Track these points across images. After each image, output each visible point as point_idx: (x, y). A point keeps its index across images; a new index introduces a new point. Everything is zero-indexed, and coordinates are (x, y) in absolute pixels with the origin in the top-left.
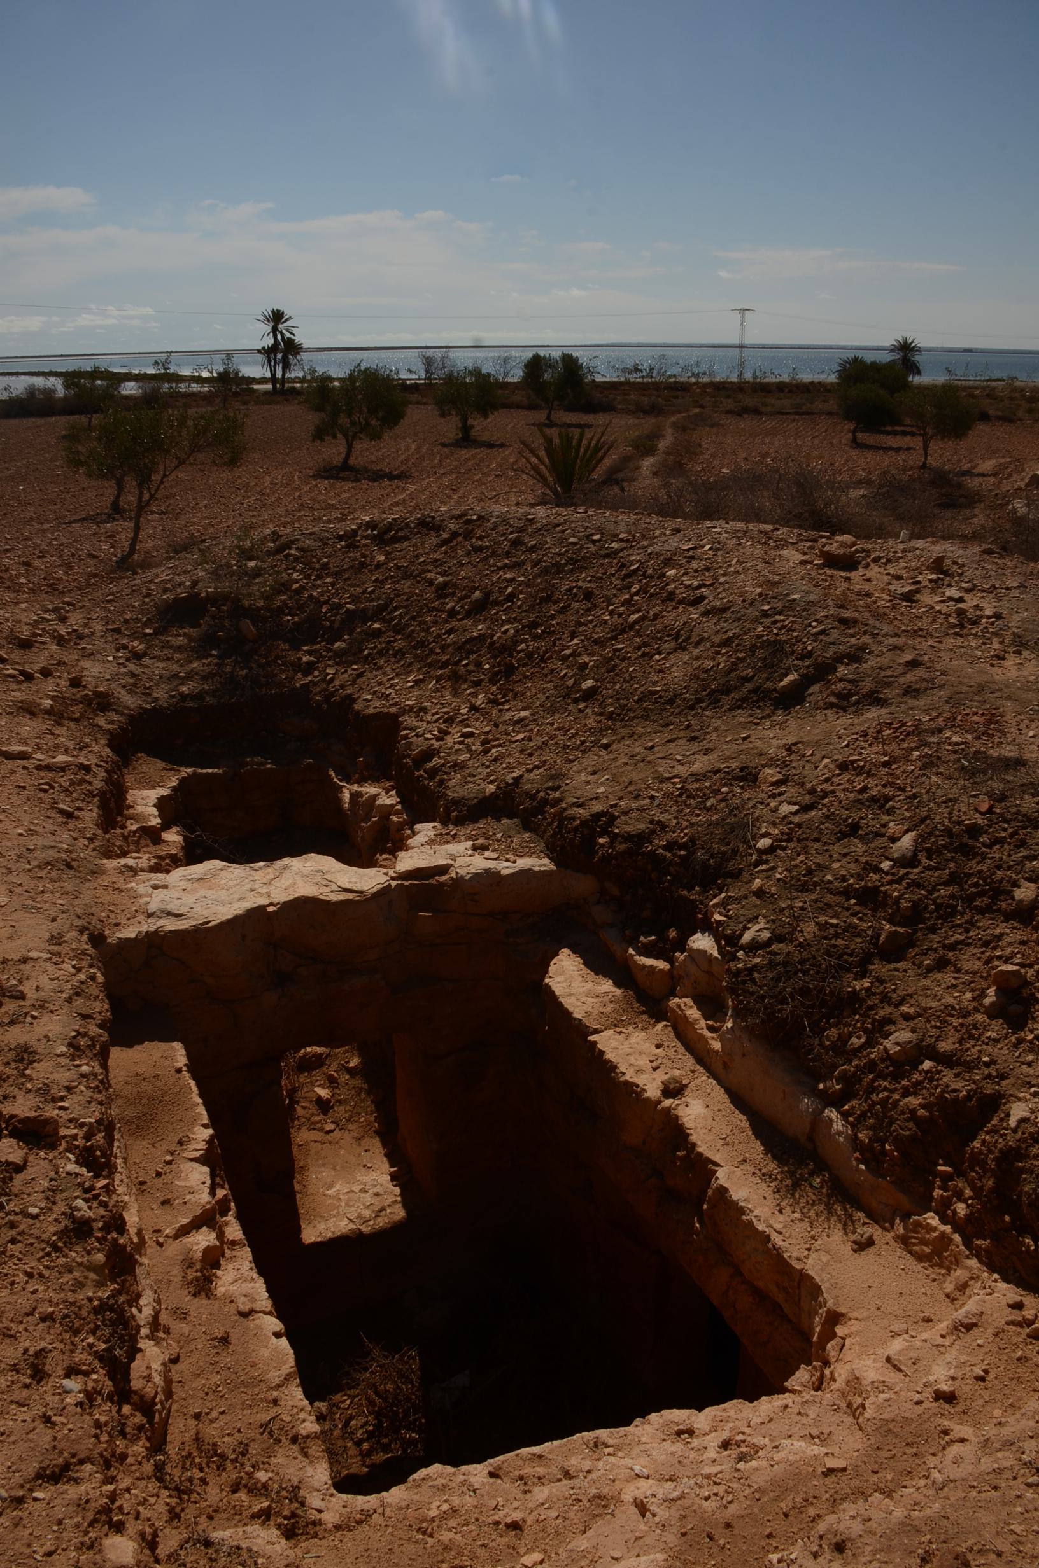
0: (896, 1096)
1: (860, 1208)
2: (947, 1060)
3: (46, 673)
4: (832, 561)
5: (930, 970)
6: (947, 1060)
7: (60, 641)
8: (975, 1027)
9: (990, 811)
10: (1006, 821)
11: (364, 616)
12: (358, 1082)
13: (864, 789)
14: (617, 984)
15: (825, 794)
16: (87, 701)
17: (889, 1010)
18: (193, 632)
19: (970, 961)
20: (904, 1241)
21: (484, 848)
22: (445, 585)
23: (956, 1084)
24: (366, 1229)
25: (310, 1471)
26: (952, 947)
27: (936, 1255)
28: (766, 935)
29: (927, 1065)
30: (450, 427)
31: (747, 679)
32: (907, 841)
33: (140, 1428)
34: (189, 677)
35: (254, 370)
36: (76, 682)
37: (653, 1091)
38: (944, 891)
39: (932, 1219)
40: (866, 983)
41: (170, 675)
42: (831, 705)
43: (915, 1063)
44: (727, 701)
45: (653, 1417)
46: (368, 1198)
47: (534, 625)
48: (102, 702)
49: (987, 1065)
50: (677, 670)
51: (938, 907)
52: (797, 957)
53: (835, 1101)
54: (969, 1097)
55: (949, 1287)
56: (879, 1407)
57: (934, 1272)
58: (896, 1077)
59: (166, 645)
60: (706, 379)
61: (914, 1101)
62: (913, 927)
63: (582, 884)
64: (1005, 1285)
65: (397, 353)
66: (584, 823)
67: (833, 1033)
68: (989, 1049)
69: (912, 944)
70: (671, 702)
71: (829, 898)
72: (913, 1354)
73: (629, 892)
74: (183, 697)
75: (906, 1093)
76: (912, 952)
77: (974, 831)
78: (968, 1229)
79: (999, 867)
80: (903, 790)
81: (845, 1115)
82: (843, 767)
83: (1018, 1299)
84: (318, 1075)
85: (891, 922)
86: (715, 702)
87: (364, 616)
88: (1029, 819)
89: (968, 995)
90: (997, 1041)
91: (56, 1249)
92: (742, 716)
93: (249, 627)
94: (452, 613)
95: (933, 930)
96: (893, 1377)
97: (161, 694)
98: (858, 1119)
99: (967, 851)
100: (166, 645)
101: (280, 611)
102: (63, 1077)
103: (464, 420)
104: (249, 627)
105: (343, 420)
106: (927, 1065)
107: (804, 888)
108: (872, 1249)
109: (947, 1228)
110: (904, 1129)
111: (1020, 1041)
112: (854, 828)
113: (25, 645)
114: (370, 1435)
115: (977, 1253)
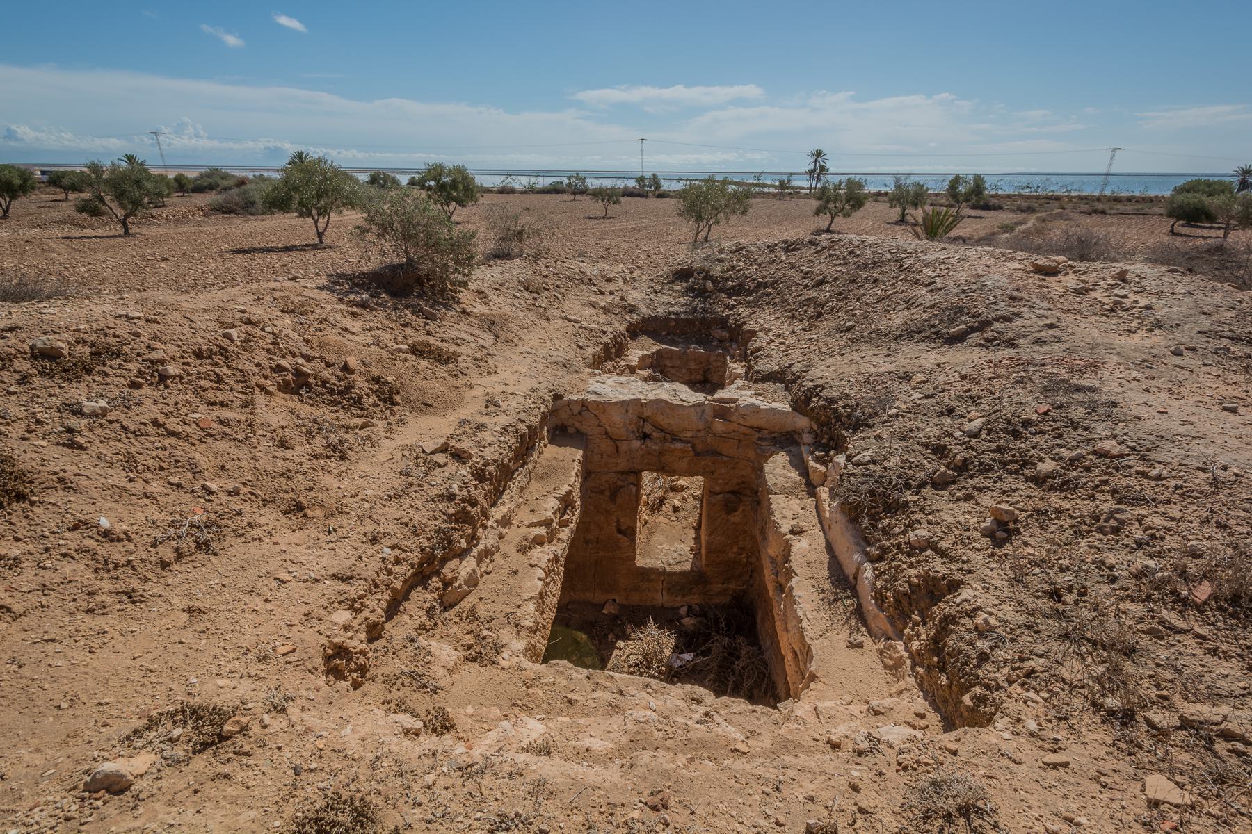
0: (905, 566)
1: (866, 625)
2: (942, 553)
3: (611, 293)
4: (1039, 270)
5: (958, 499)
6: (942, 553)
7: (625, 281)
8: (968, 538)
9: (1046, 413)
10: (1055, 421)
11: (766, 285)
12: (696, 503)
13: (969, 390)
14: (800, 475)
15: (943, 391)
16: (624, 308)
17: (922, 515)
18: (684, 284)
19: (987, 500)
20: (881, 653)
21: (759, 395)
22: (807, 273)
23: (939, 567)
24: (668, 569)
25: (514, 641)
26: (980, 490)
27: (894, 668)
28: (868, 458)
29: (929, 552)
30: (895, 213)
31: (933, 326)
32: (977, 423)
33: (437, 589)
34: (676, 304)
35: (802, 183)
36: (622, 299)
37: (785, 528)
38: (987, 456)
39: (900, 646)
40: (916, 498)
41: (673, 302)
42: (980, 345)
43: (922, 550)
44: (917, 337)
45: (688, 687)
46: (675, 555)
47: (840, 294)
48: (632, 309)
49: (964, 562)
50: (899, 319)
51: (981, 464)
52: (879, 473)
53: (874, 560)
54: (944, 578)
55: (894, 690)
56: (791, 731)
57: (890, 678)
58: (909, 555)
59: (671, 289)
60: (1075, 194)
61: (913, 572)
62: (956, 472)
63: (802, 422)
64: (923, 701)
65: (880, 177)
66: (809, 389)
67: (886, 522)
68: (970, 553)
69: (954, 482)
70: (886, 335)
71: (916, 447)
72: (832, 713)
73: (825, 426)
74: (670, 313)
75: (912, 566)
76: (952, 487)
77: (1027, 423)
78: (917, 658)
79: (1034, 448)
80: (993, 394)
81: (875, 569)
82: (963, 377)
83: (922, 711)
84: (679, 496)
85: (948, 467)
86: (910, 337)
87: (766, 285)
88: (1072, 423)
89: (975, 519)
90: (979, 550)
91: (433, 500)
92: (922, 346)
93: (709, 285)
94: (806, 286)
95: (971, 477)
96: (812, 719)
97: (661, 311)
98: (881, 574)
99: (1016, 434)
100: (671, 289)
101: (727, 279)
102: (490, 439)
103: (904, 210)
104: (709, 285)
105: (831, 205)
106: (929, 552)
107: (903, 439)
108: (859, 650)
109: (906, 654)
110: (902, 586)
111: (993, 554)
112: (951, 411)
113: (609, 280)
114: (637, 665)
115: (915, 675)
